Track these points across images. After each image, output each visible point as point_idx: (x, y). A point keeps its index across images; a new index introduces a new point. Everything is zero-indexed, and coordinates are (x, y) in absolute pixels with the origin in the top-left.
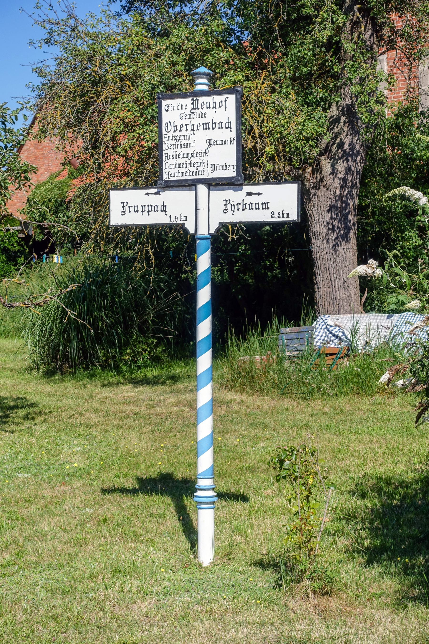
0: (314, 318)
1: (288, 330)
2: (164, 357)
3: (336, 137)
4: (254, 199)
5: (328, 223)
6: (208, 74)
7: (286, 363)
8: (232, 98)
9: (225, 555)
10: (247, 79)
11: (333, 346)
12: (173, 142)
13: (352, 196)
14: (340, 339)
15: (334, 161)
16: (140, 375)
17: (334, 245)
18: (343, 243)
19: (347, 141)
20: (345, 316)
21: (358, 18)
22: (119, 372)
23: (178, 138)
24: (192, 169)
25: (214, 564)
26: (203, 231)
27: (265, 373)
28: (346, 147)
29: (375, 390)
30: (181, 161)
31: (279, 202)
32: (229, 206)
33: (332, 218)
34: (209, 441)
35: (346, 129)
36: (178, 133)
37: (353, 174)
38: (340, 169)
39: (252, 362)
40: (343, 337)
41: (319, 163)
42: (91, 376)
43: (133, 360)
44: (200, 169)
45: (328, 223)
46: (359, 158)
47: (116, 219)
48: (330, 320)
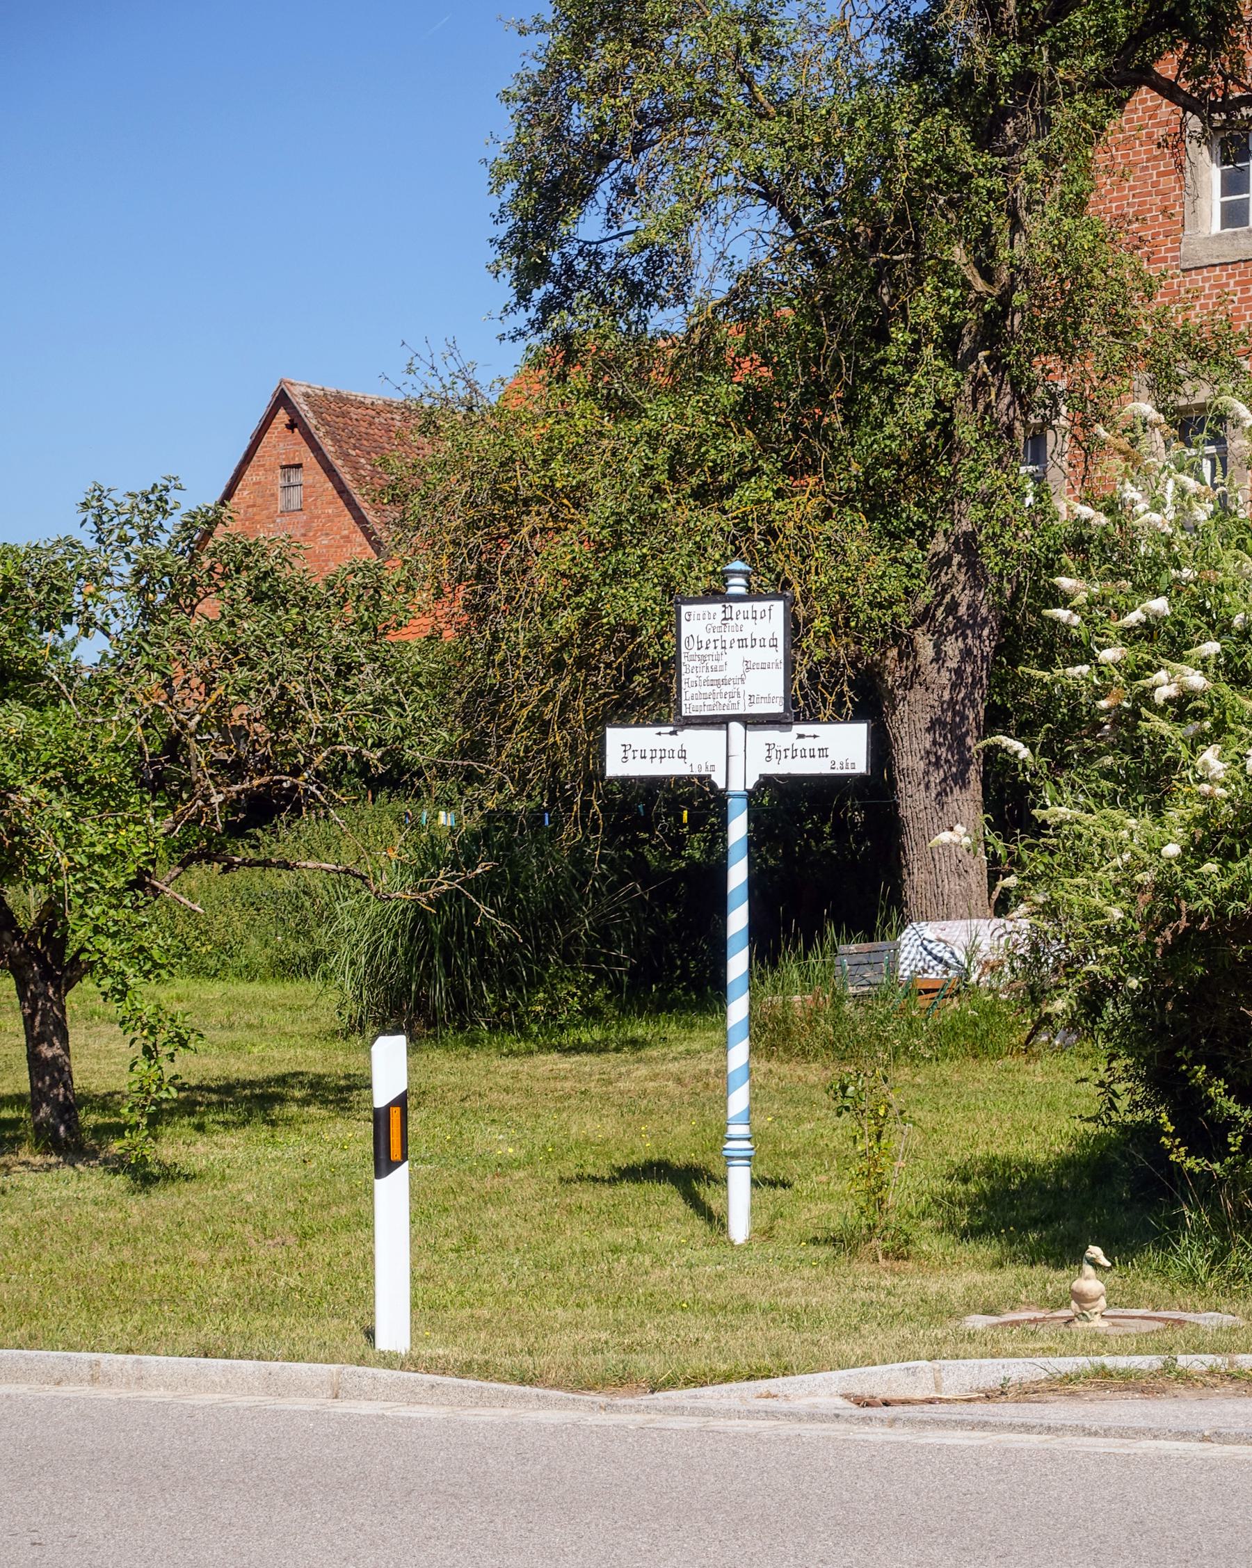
0: (901, 928)
1: (853, 948)
2: (610, 1010)
3: (944, 592)
4: (807, 743)
5: (928, 753)
6: (746, 572)
7: (848, 1006)
8: (779, 606)
9: (764, 1233)
10: (779, 494)
11: (933, 976)
12: (697, 663)
13: (973, 701)
14: (947, 964)
15: (940, 636)
16: (568, 1039)
17: (939, 794)
18: (956, 790)
19: (964, 600)
20: (957, 923)
21: (984, 374)
22: (526, 1035)
23: (703, 659)
24: (723, 701)
25: (749, 1241)
26: (737, 786)
27: (809, 1023)
28: (962, 610)
29: (1005, 1049)
30: (708, 690)
31: (841, 748)
32: (773, 753)
33: (934, 743)
34: (745, 1073)
35: (962, 578)
36: (703, 652)
37: (975, 662)
38: (950, 653)
39: (786, 1004)
40: (952, 961)
41: (911, 641)
42: (473, 1042)
43: (549, 1014)
44: (734, 700)
45: (928, 753)
46: (986, 632)
47: (615, 767)
48: (930, 930)
